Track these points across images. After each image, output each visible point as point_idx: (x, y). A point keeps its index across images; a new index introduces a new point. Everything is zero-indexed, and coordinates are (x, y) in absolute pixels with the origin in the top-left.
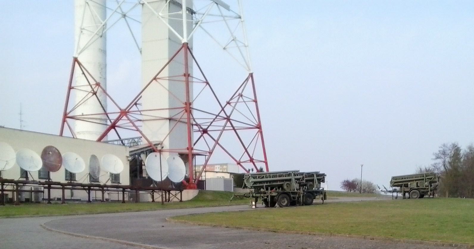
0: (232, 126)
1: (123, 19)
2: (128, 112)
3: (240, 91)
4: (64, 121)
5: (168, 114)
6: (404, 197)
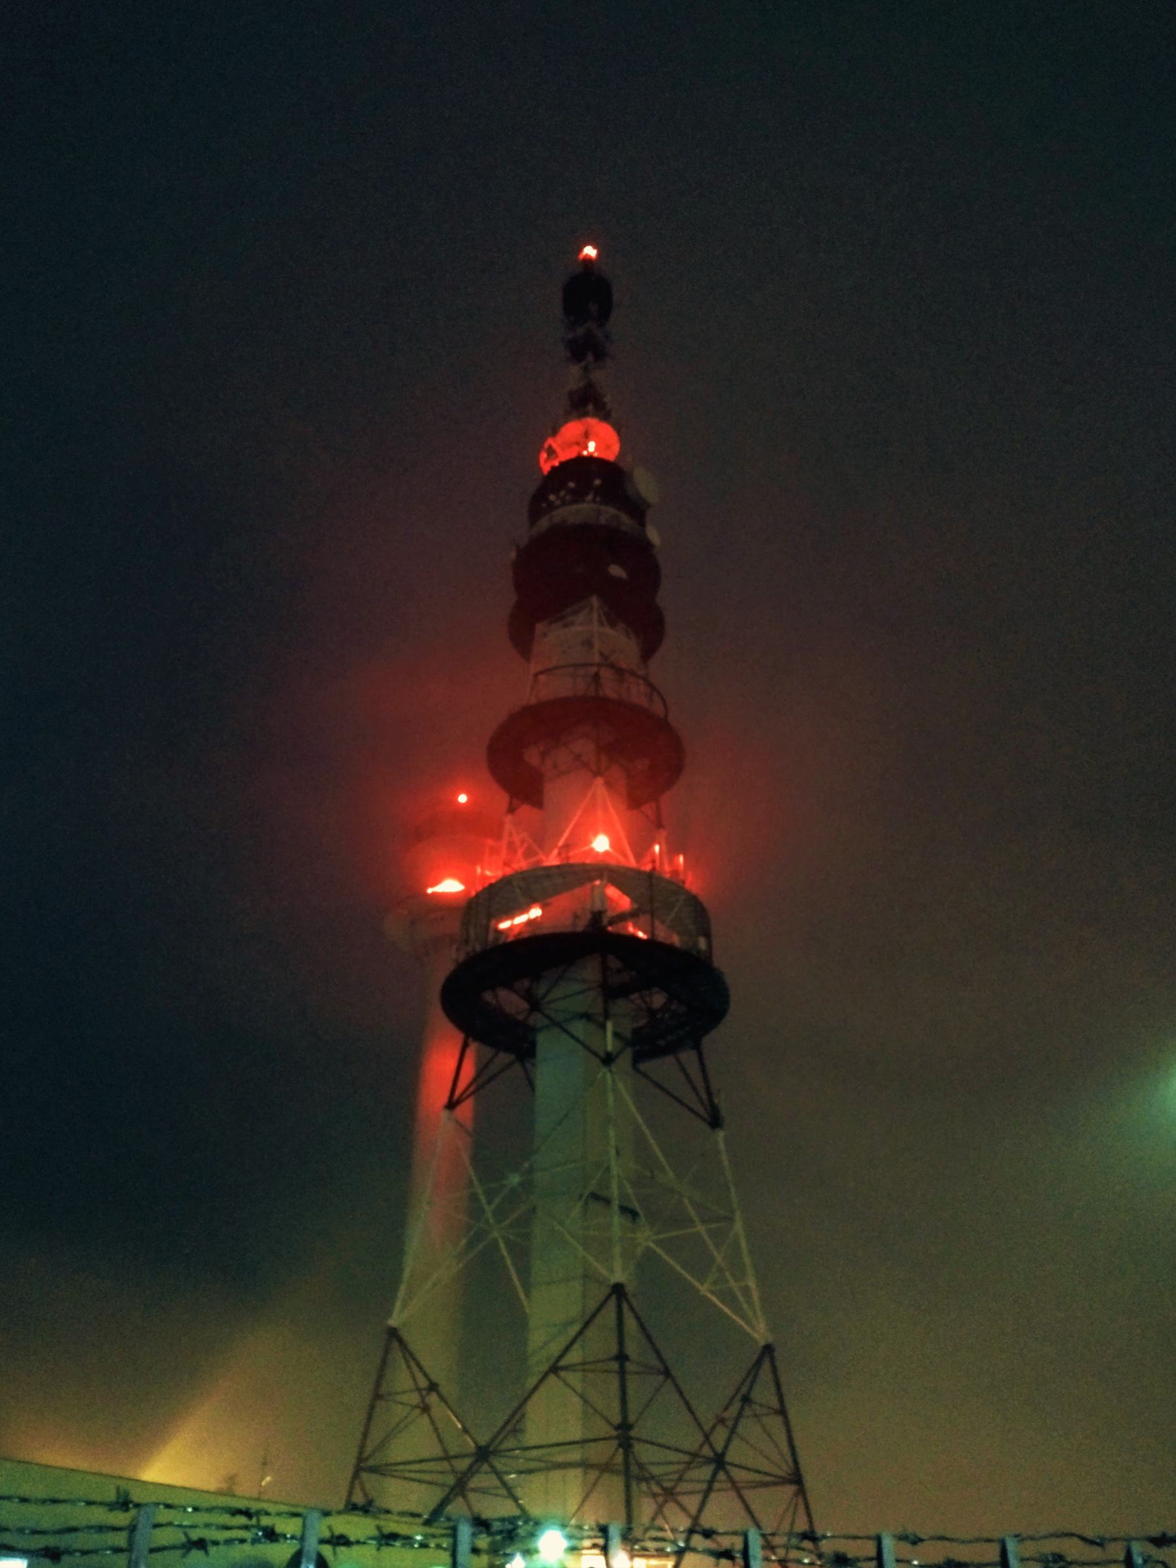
2: (496, 1452)
3: (744, 1390)
4: (356, 1475)
6: (764, 1411)
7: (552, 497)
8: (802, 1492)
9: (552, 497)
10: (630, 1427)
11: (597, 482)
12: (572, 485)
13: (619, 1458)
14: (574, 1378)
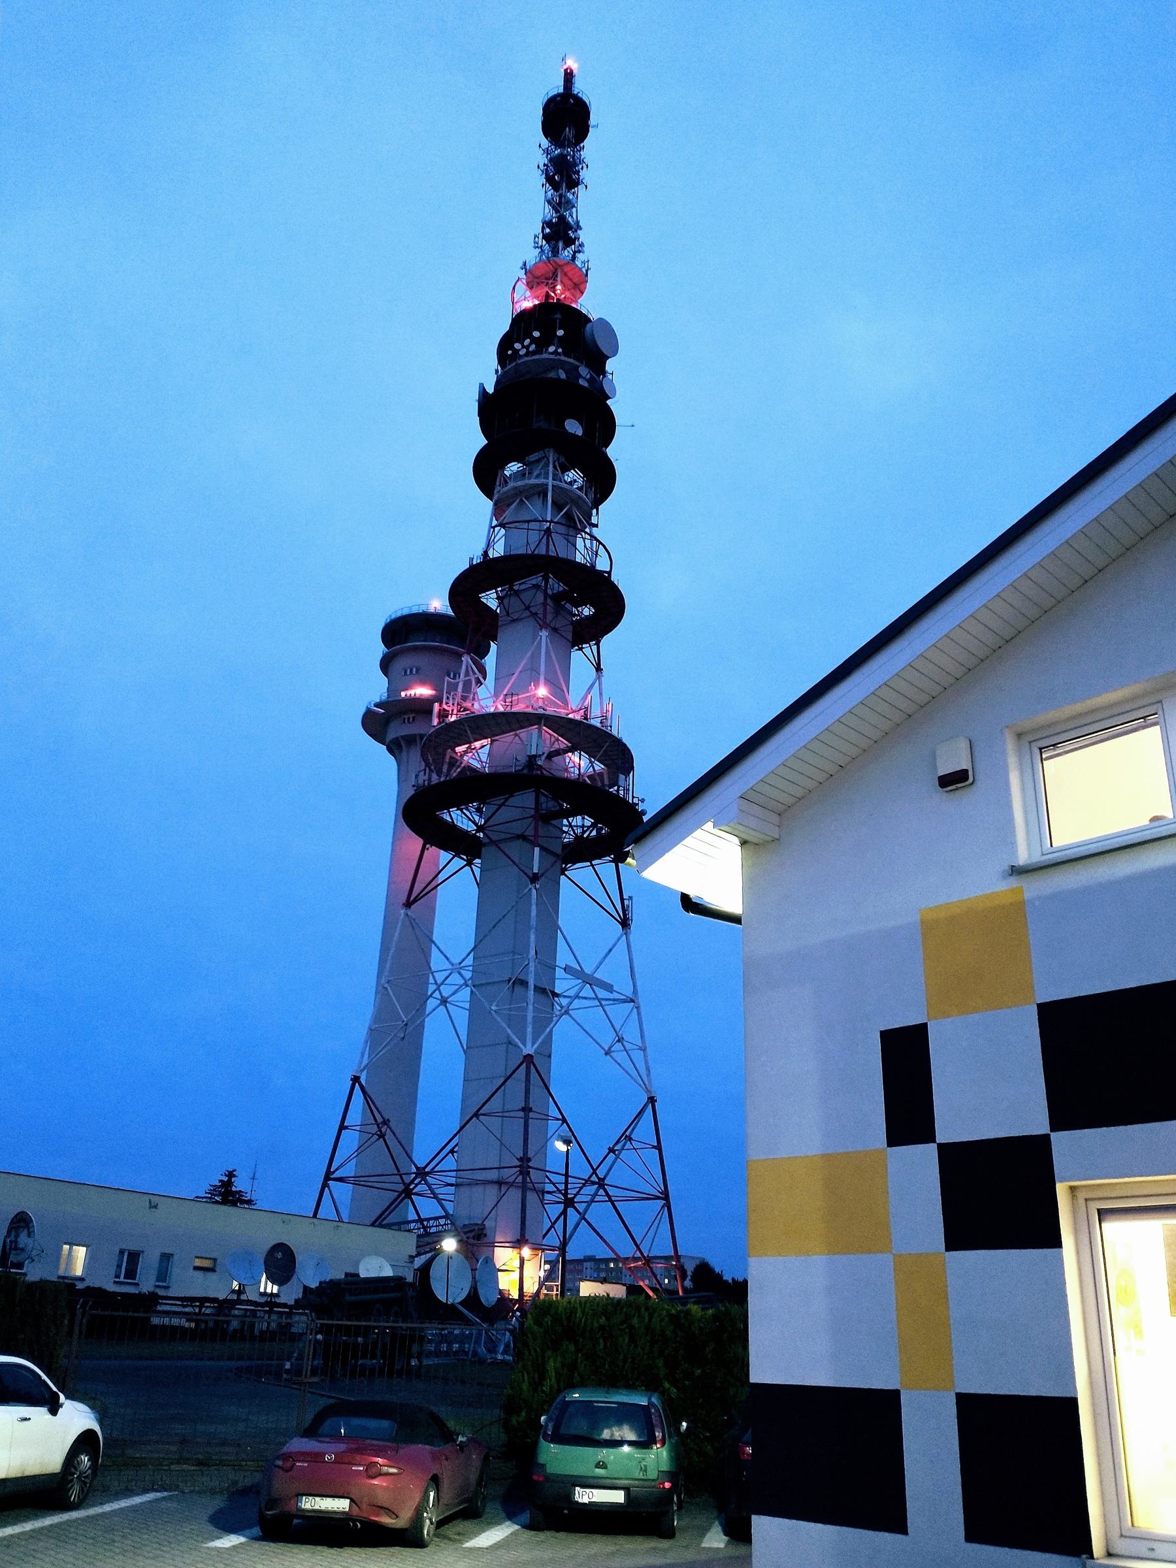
0: (607, 1194)
1: (442, 1008)
4: (325, 1185)
5: (487, 1533)
7: (517, 346)
8: (668, 1205)
9: (517, 346)
10: (529, 1160)
11: (560, 333)
12: (536, 334)
13: (520, 1179)
14: (494, 1123)
